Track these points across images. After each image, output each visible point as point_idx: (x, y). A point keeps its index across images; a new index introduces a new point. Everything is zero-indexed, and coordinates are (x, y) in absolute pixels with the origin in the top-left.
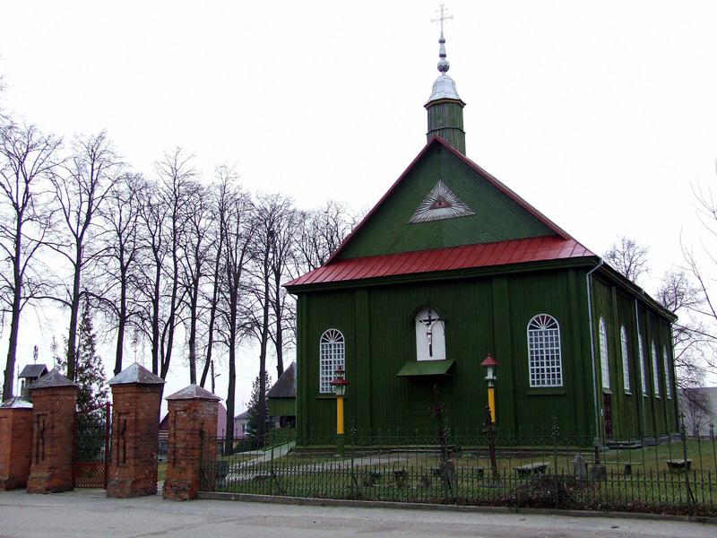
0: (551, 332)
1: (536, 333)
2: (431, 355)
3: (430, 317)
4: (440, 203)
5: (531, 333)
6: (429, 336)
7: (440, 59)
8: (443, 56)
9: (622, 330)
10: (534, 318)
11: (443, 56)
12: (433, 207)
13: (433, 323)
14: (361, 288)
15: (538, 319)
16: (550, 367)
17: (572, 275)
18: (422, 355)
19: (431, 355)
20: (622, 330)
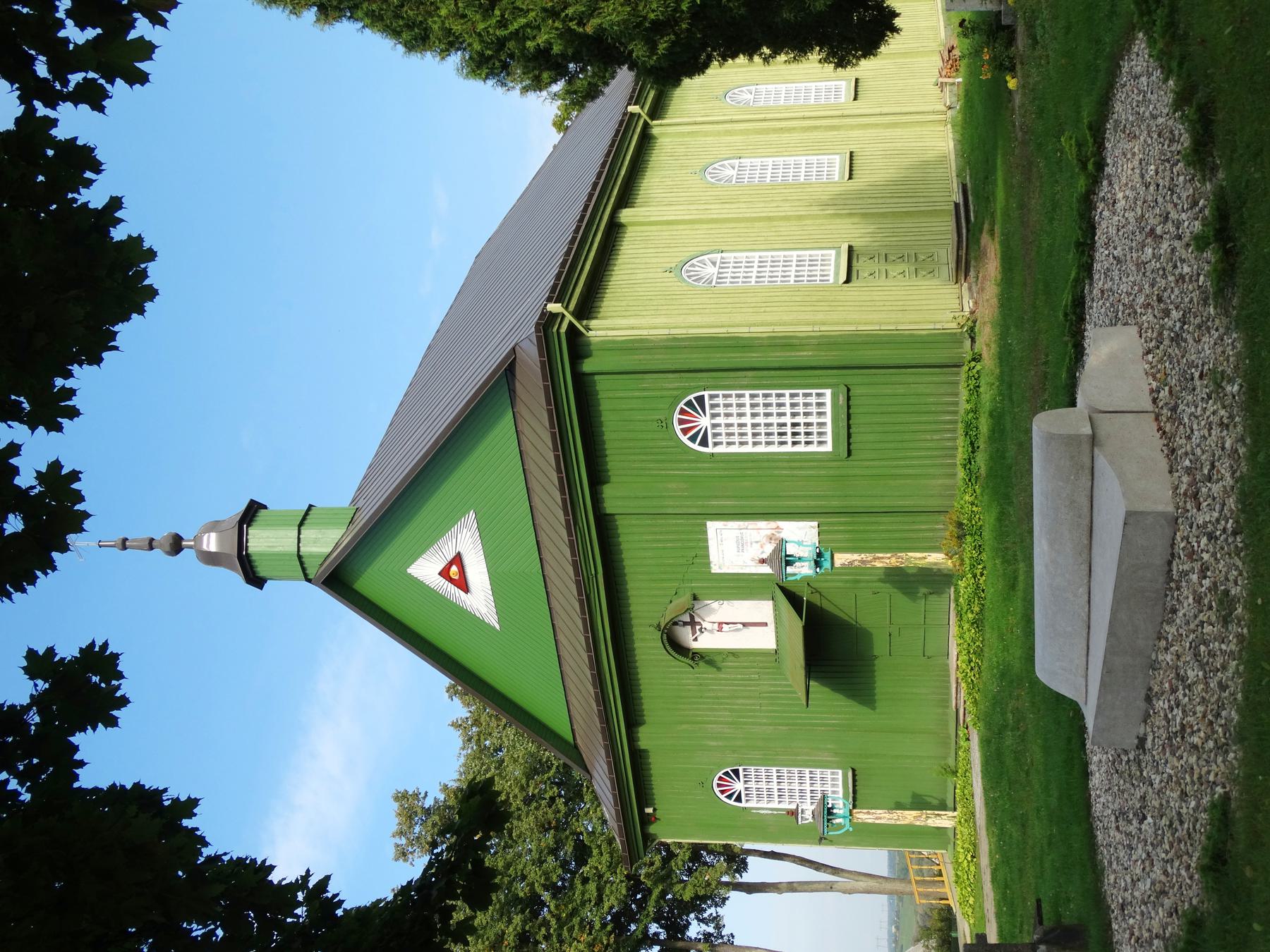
0: (713, 406)
1: (715, 435)
2: (766, 624)
3: (685, 624)
4: (456, 572)
5: (716, 444)
6: (725, 627)
7: (157, 551)
8: (151, 545)
9: (63, 404)
10: (685, 439)
11: (151, 545)
12: (463, 585)
13: (697, 619)
14: (632, 739)
15: (685, 431)
16: (761, 420)
17: (588, 366)
18: (764, 640)
19: (766, 624)
20: (63, 404)
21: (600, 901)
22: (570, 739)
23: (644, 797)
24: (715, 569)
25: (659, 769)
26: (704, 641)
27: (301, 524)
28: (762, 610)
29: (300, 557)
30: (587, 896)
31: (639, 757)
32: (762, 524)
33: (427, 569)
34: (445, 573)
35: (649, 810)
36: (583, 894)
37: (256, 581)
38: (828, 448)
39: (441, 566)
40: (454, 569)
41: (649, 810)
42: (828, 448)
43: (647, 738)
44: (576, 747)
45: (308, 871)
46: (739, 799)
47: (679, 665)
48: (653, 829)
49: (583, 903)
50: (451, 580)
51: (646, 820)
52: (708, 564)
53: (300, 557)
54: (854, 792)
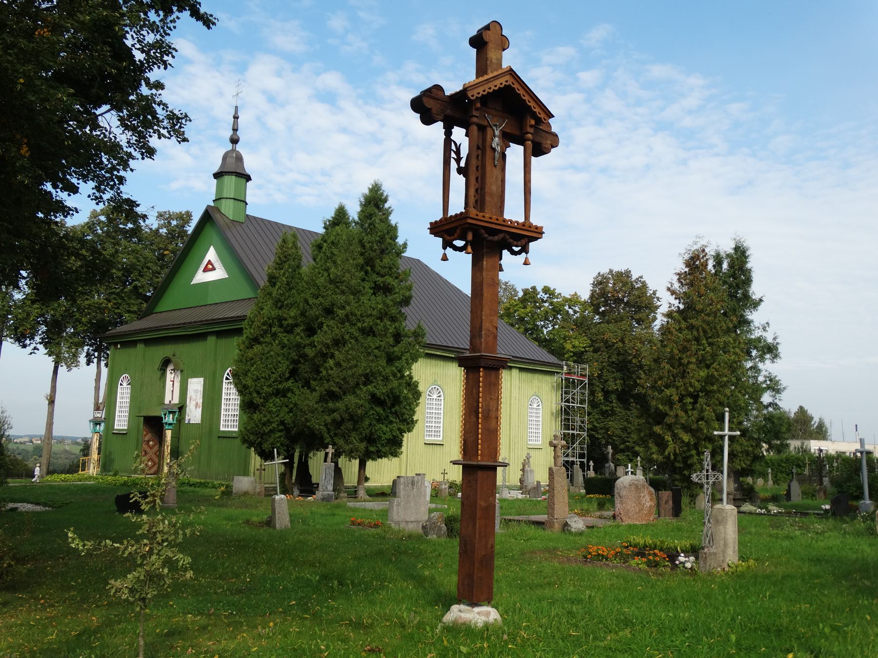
4: (208, 269)
21: (129, 312)
22: (156, 311)
23: (125, 345)
24: (190, 380)
25: (131, 351)
26: (169, 376)
27: (234, 199)
28: (176, 401)
29: (220, 199)
30: (131, 306)
31: (134, 344)
32: (201, 401)
33: (211, 255)
34: (209, 262)
35: (119, 346)
36: (133, 304)
37: (217, 176)
38: (222, 429)
39: (212, 261)
40: (210, 267)
41: (119, 346)
42: (222, 429)
43: (141, 347)
44: (152, 314)
45: (185, 140)
46: (121, 385)
47: (158, 364)
48: (112, 348)
49: (128, 304)
50: (207, 265)
51: (115, 344)
52: (191, 378)
53: (220, 199)
54: (120, 434)
